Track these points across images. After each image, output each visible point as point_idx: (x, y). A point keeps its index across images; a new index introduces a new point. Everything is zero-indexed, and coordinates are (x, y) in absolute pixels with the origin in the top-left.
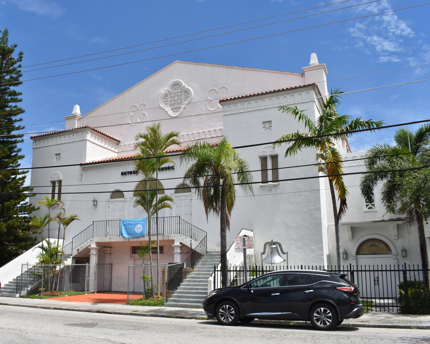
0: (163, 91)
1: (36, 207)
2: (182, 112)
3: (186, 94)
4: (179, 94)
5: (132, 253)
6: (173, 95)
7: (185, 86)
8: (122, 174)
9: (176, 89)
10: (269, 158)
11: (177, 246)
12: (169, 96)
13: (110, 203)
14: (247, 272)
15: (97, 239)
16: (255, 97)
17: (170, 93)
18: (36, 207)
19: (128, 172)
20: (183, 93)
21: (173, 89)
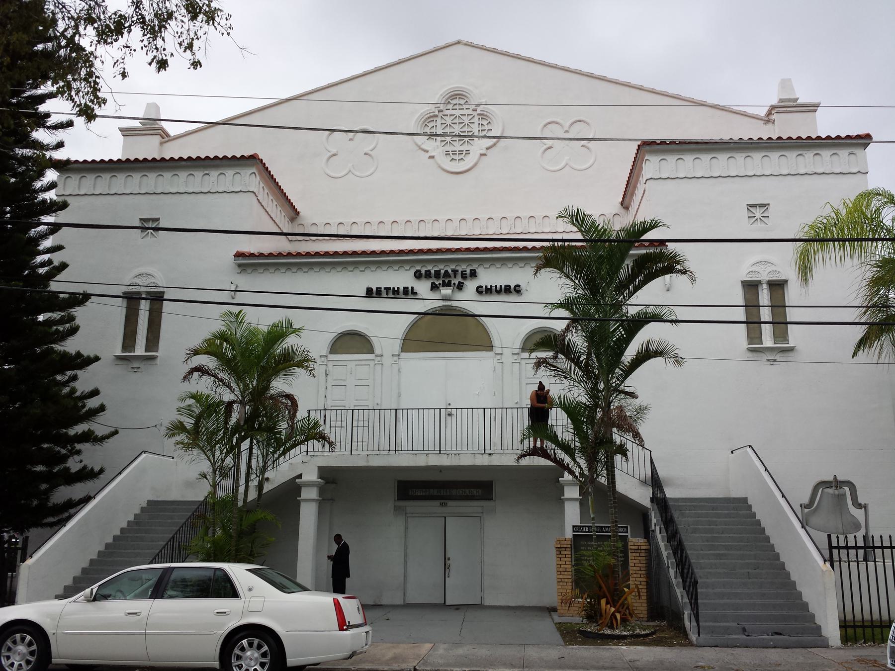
1: (97, 469)
3: (485, 122)
4: (466, 120)
5: (399, 499)
6: (448, 120)
10: (765, 286)
11: (310, 484)
12: (439, 121)
13: (330, 364)
18: (97, 469)
19: (387, 289)
20: (476, 120)
21: (450, 107)
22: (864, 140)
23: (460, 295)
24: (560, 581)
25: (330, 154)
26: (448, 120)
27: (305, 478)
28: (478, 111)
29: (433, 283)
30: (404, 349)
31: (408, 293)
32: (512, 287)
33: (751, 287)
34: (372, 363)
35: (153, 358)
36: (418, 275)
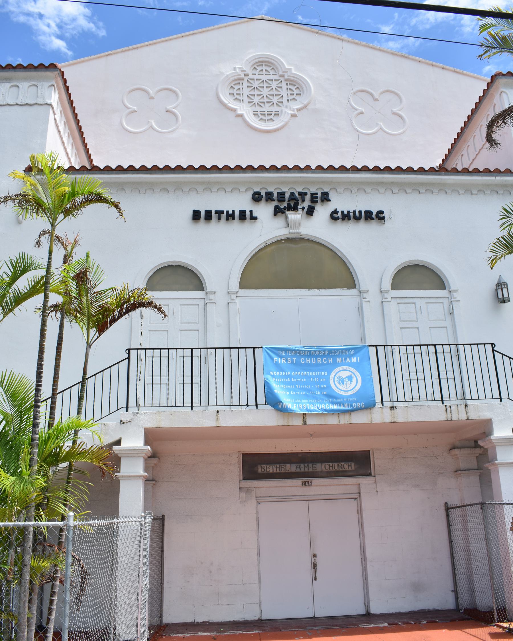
0: (227, 70)
2: (286, 124)
5: (244, 479)
7: (290, 69)
8: (196, 215)
11: (132, 453)
12: (246, 84)
15: (150, 419)
16: (467, 131)
17: (246, 78)
19: (219, 213)
20: (284, 85)
26: (256, 84)
27: (125, 445)
30: (244, 285)
32: (374, 213)
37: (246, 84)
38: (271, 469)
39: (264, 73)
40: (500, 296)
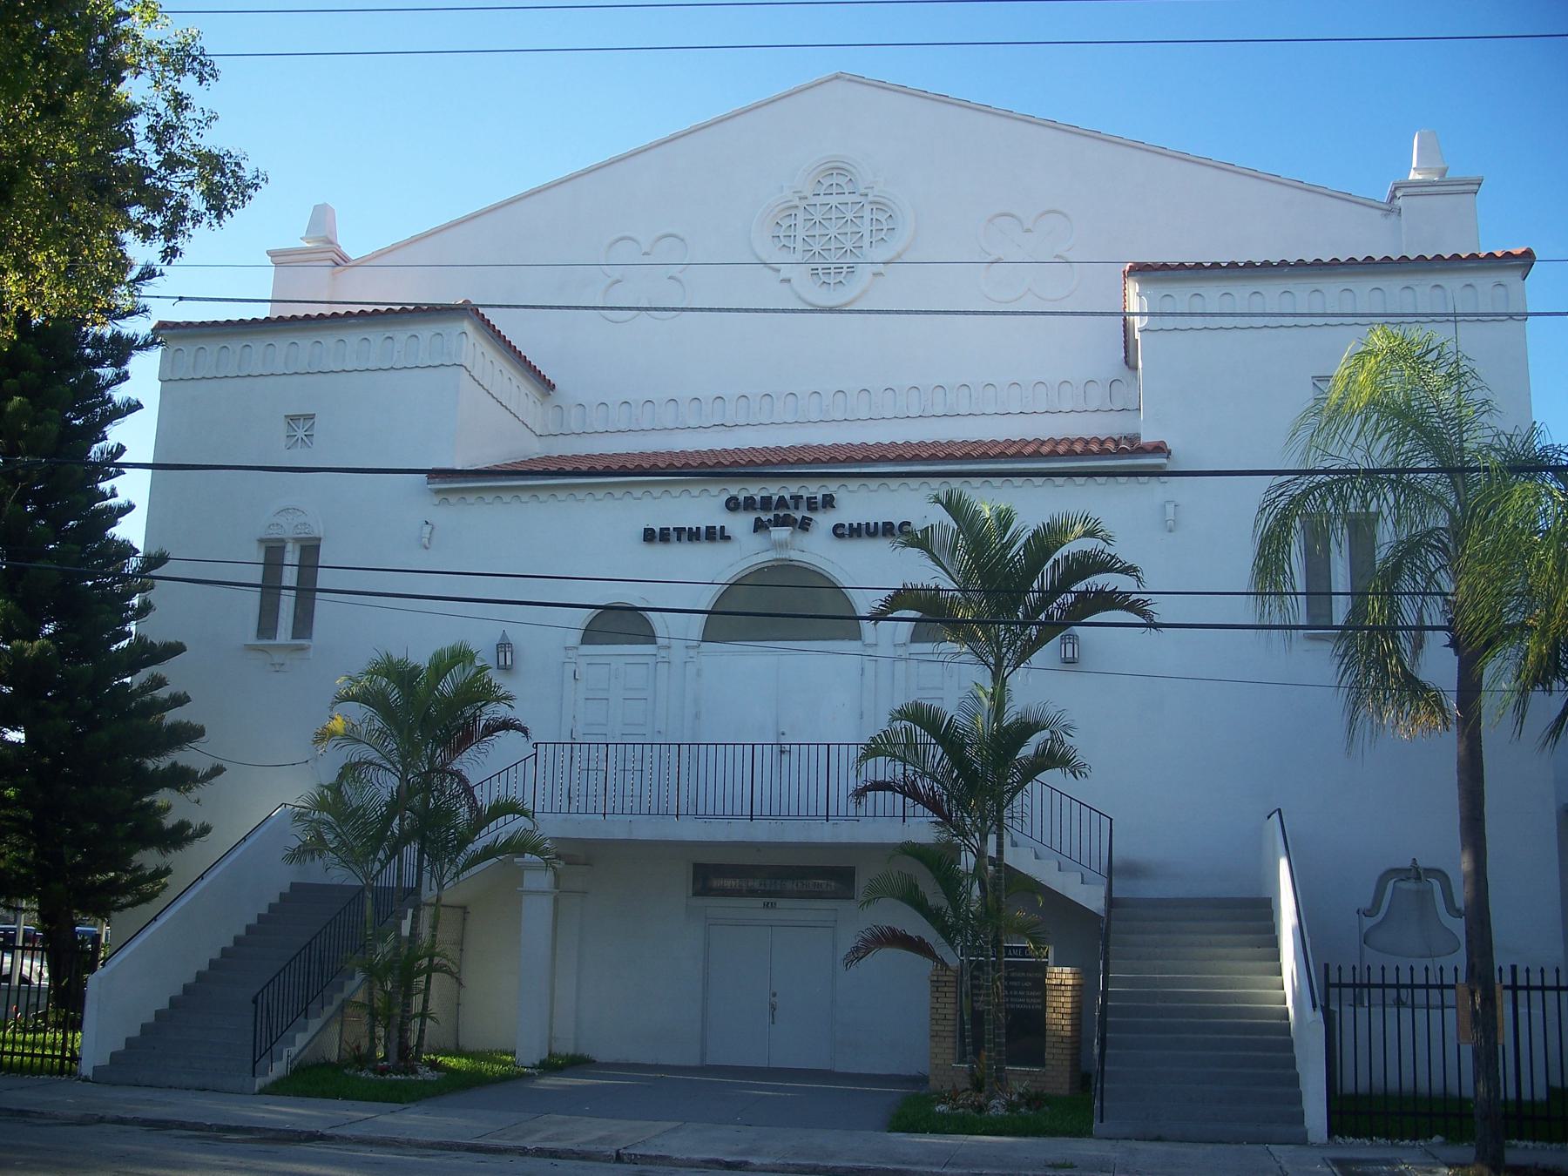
3: (883, 217)
9: (834, 190)
12: (801, 216)
14: (1331, 990)
19: (680, 531)
22: (1526, 259)
23: (803, 540)
24: (934, 1036)
25: (609, 281)
28: (870, 198)
29: (758, 520)
31: (714, 535)
33: (273, 554)
34: (651, 660)
35: (302, 648)
36: (732, 505)
37: (801, 216)
38: (729, 883)
39: (834, 190)
40: (502, 662)
